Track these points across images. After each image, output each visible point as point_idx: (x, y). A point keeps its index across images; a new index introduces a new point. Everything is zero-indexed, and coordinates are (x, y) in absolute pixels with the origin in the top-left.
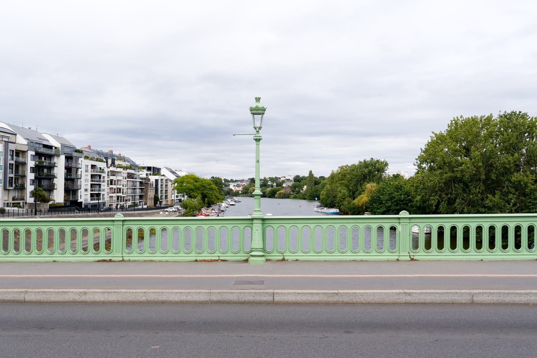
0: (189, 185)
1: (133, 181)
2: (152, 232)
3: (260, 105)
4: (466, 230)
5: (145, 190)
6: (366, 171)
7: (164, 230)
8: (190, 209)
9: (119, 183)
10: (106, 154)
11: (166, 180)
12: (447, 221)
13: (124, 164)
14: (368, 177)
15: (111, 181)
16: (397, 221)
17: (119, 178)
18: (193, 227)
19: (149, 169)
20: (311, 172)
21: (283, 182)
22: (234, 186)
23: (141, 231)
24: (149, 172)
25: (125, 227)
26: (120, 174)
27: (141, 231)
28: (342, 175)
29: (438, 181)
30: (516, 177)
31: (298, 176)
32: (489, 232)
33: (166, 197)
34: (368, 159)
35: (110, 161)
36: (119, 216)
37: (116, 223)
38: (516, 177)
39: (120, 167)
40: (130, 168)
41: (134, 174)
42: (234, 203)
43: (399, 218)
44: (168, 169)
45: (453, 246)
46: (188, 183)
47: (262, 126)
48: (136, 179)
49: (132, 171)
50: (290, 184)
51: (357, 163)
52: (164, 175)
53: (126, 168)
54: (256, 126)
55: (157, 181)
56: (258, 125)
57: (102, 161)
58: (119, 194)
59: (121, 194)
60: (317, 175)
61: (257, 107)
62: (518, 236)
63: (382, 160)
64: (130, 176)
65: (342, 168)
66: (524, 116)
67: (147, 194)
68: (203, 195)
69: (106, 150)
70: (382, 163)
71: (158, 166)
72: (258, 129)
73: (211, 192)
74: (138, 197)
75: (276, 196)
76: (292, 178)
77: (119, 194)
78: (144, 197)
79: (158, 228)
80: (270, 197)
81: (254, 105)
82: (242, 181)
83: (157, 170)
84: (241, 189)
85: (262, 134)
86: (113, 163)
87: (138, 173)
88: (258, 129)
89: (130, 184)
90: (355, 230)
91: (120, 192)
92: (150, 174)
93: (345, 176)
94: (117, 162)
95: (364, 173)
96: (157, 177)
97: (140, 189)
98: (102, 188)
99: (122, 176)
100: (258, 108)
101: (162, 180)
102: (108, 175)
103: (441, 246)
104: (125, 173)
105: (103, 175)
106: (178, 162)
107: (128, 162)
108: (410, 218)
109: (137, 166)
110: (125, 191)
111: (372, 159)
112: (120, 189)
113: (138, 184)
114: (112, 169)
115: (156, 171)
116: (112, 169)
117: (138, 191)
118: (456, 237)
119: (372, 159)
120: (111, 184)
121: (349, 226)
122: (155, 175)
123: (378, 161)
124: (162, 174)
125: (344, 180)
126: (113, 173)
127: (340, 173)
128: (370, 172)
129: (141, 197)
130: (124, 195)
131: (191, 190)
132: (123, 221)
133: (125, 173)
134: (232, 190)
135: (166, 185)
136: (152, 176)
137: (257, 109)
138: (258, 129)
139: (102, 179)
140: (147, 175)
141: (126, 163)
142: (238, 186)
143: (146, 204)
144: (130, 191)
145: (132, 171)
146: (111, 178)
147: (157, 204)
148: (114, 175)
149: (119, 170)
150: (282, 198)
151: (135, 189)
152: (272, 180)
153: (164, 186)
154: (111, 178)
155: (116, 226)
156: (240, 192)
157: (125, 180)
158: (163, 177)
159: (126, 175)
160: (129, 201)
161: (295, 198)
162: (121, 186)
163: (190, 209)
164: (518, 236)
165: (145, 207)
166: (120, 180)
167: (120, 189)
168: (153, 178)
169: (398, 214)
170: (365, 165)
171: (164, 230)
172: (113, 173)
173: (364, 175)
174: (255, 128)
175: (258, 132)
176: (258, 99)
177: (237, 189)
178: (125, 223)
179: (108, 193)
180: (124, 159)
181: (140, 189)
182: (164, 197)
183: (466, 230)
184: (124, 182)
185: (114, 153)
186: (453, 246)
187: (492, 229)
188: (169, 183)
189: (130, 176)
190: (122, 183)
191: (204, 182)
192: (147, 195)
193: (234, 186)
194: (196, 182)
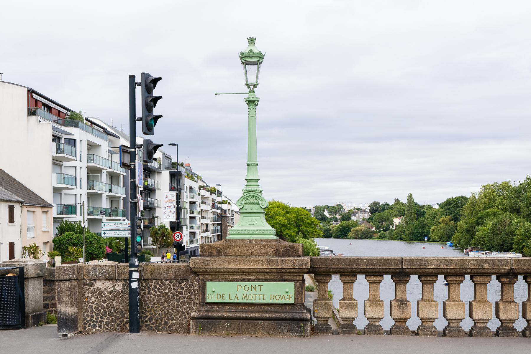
3: (257, 48)
21: (351, 213)
28: (490, 199)
31: (376, 204)
47: (259, 83)
50: (367, 216)
54: (249, 82)
56: (252, 80)
60: (420, 200)
61: (251, 51)
66: (506, 186)
72: (252, 87)
75: (350, 235)
76: (366, 206)
80: (338, 237)
81: (245, 48)
85: (258, 93)
88: (252, 87)
93: (495, 200)
100: (253, 53)
137: (251, 55)
138: (252, 86)
150: (361, 238)
152: (333, 210)
161: (382, 237)
174: (248, 86)
175: (252, 91)
176: (252, 41)
194: (287, 212)
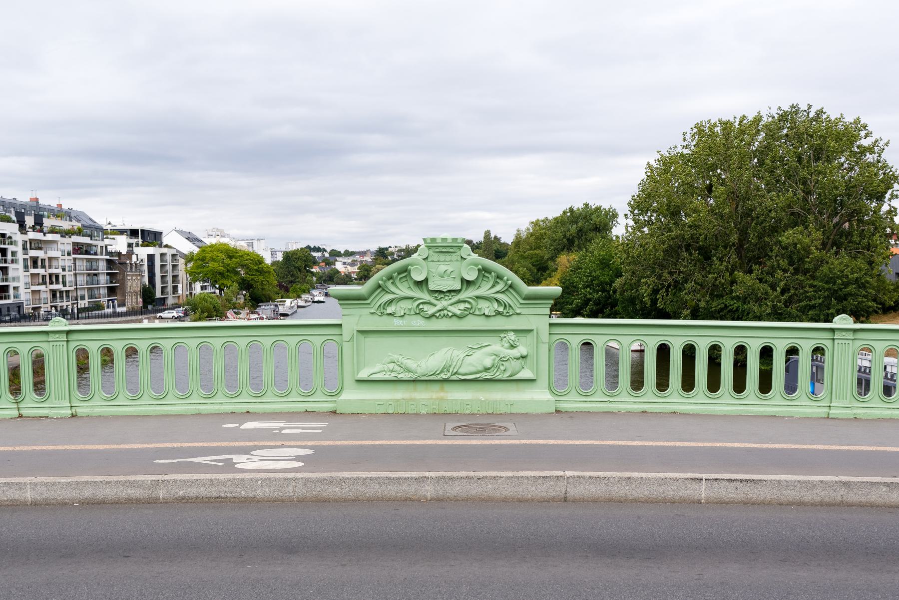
0: (216, 265)
1: (88, 260)
2: (131, 352)
4: (689, 353)
5: (119, 277)
6: (573, 229)
7: (154, 349)
8: (203, 312)
9: (54, 263)
10: (23, 205)
11: (173, 255)
12: (677, 334)
13: (65, 225)
14: (576, 243)
15: (35, 261)
16: (828, 335)
17: (52, 254)
18: (217, 342)
19: (134, 233)
20: (488, 233)
22: (344, 263)
23: (107, 353)
24: (134, 241)
25: (73, 345)
26: (55, 246)
27: (107, 353)
28: (537, 238)
29: (654, 247)
30: (788, 236)
32: (746, 358)
33: (175, 289)
34: (578, 205)
35: (29, 221)
36: (60, 324)
37: (51, 338)
38: (788, 236)
39: (53, 231)
40: (79, 233)
41: (90, 245)
42: (322, 298)
43: (833, 330)
44: (181, 233)
45: (739, 385)
46: (213, 260)
48: (96, 254)
49: (87, 240)
51: (558, 213)
52: (167, 246)
53: (65, 234)
55: (151, 258)
57: (9, 220)
58: (54, 287)
59: (60, 287)
62: (740, 366)
63: (605, 206)
64: (78, 249)
65: (536, 224)
67: (123, 284)
68: (247, 283)
69: (24, 197)
70: (607, 213)
71: (156, 228)
73: (261, 278)
74: (104, 291)
77: (54, 287)
78: (118, 291)
79: (143, 346)
82: (363, 254)
83: (152, 236)
84: (356, 269)
86: (39, 222)
87: (100, 243)
89: (82, 266)
90: (204, 350)
91: (58, 282)
92: (137, 245)
94: (47, 223)
95: (568, 234)
96: (150, 250)
97: (108, 274)
98: (11, 274)
99: (59, 250)
101: (162, 255)
102: (24, 249)
103: (662, 384)
104: (66, 243)
105: (11, 248)
106: (194, 217)
107: (79, 221)
108: (855, 331)
109: (100, 229)
110: (68, 279)
111: (587, 205)
112: (57, 276)
113: (102, 266)
114: (32, 235)
115: (151, 237)
116: (32, 235)
117: (103, 279)
118: (744, 366)
119: (587, 205)
120: (35, 265)
121: (192, 344)
122: (147, 246)
123: (598, 209)
124: (165, 243)
125: (539, 248)
126: (37, 245)
127: (532, 235)
128: (581, 230)
129: (111, 291)
130: (67, 288)
131: (220, 273)
132: (68, 332)
133: (66, 243)
134: (338, 272)
135: (174, 267)
136: (140, 248)
139: (9, 257)
140: (130, 245)
141: (74, 223)
142: (353, 264)
143: (122, 304)
144: (82, 280)
145: (87, 240)
146: (33, 253)
147: (151, 302)
148: (40, 249)
149: (50, 237)
151: (96, 275)
153: (169, 268)
154: (33, 253)
155: (55, 343)
156: (354, 276)
157: (66, 257)
158: (164, 250)
159: (70, 248)
160: (83, 298)
162: (59, 271)
163: (203, 312)
164: (740, 366)
165: (124, 309)
166: (57, 258)
167: (57, 276)
168: (142, 253)
169: (828, 320)
170: (572, 217)
171: (154, 349)
172: (37, 245)
173: (568, 240)
177: (350, 269)
178: (72, 337)
179: (26, 284)
180: (68, 215)
181: (108, 274)
182: (170, 289)
183: (689, 353)
184: (67, 261)
185: (40, 202)
186: (739, 385)
187: (741, 351)
188: (181, 262)
189: (78, 249)
190: (61, 263)
191: (246, 257)
192: (129, 284)
193: (344, 263)
